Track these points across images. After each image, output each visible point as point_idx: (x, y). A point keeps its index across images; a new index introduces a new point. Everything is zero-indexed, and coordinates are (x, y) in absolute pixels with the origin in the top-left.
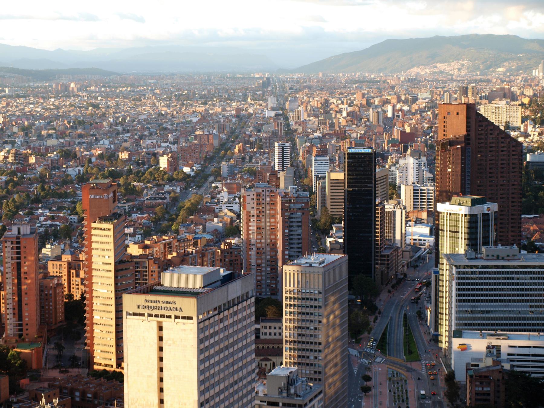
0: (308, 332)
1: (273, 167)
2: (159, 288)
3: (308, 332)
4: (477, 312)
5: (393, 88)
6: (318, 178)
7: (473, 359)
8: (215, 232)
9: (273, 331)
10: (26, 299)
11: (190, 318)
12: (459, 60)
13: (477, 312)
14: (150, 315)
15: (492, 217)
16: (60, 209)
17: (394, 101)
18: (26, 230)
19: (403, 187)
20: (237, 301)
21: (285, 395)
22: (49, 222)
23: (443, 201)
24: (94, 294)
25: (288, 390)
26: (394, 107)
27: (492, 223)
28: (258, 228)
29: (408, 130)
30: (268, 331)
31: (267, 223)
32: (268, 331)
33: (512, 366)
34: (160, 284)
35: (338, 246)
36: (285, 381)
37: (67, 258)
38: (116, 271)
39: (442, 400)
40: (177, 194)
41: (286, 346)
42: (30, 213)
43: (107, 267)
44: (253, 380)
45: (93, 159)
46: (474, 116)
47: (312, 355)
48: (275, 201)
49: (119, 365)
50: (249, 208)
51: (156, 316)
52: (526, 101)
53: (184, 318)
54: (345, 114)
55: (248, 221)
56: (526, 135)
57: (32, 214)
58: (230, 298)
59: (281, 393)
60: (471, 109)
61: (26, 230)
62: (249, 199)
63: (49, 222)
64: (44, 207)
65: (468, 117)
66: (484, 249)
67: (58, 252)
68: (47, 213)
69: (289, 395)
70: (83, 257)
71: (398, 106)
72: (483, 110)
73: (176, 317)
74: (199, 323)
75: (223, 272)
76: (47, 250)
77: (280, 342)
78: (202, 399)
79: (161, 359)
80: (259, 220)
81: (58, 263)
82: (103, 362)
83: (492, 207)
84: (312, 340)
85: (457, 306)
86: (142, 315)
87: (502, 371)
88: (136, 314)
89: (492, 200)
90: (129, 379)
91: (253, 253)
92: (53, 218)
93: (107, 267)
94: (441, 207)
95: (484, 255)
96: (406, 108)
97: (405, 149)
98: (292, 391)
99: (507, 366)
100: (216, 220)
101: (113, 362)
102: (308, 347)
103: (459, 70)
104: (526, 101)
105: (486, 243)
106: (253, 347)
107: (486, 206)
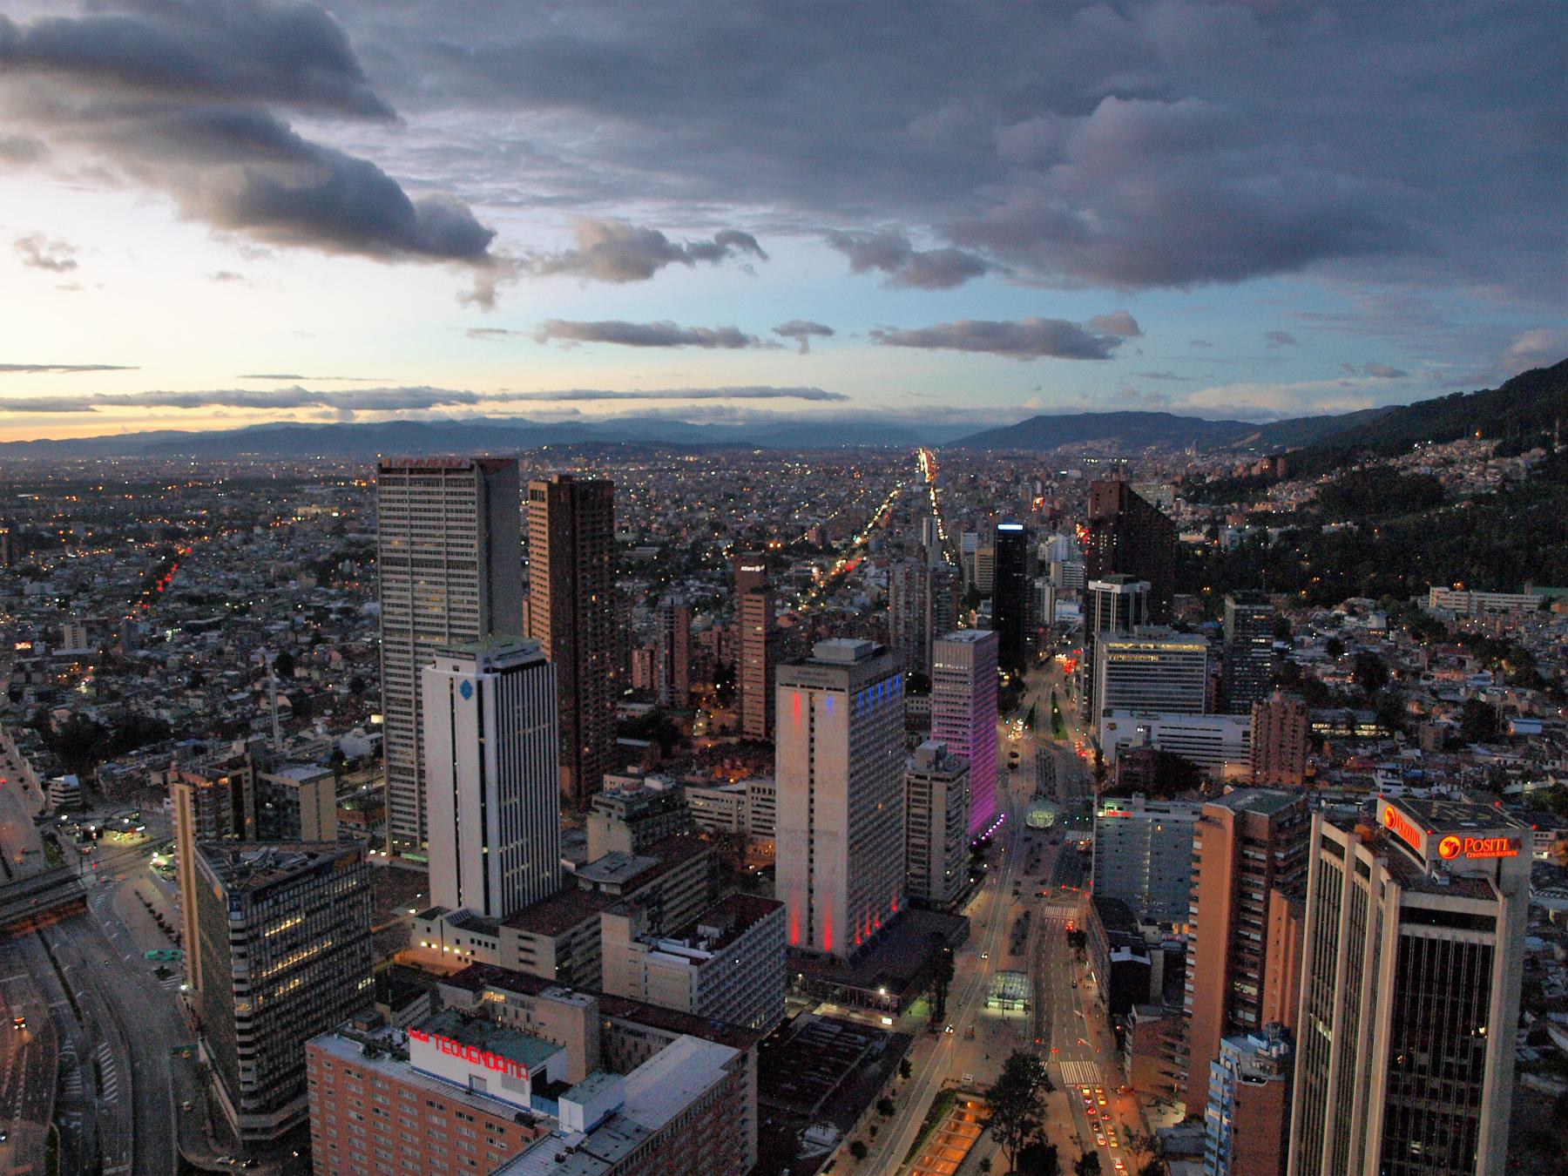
0: (957, 708)
1: (921, 543)
2: (811, 660)
3: (957, 708)
4: (1127, 692)
5: (1042, 464)
6: (966, 554)
7: (1122, 739)
8: (863, 607)
9: (919, 705)
10: (759, 629)
11: (843, 690)
12: (1109, 436)
13: (1127, 692)
14: (802, 686)
15: (1144, 597)
16: (711, 580)
17: (1044, 478)
18: (679, 600)
19: (1052, 565)
20: (885, 676)
21: (933, 768)
22: (700, 593)
23: (1095, 579)
24: (745, 664)
25: (936, 764)
26: (1043, 484)
27: (1144, 602)
28: (907, 603)
29: (1057, 507)
30: (915, 705)
31: (916, 598)
32: (915, 705)
33: (1163, 747)
34: (812, 656)
35: (986, 623)
36: (934, 754)
37: (717, 628)
38: (766, 643)
39: (1169, 803)
40: (96, 1102)
41: (935, 722)
42: (681, 584)
43: (758, 639)
44: (903, 753)
45: (743, 532)
46: (1125, 492)
47: (960, 730)
48: (199, 839)
49: (767, 734)
50: (898, 582)
51: (809, 687)
52: (1178, 479)
53: (835, 690)
54: (993, 490)
55: (897, 596)
56: (1178, 514)
57: (683, 584)
58: (881, 671)
59: (929, 767)
60: (1123, 486)
61: (679, 600)
62: (898, 574)
63: (700, 593)
64: (697, 578)
65: (1121, 496)
66: (1136, 628)
67: (708, 623)
68: (698, 583)
69: (937, 769)
70: (734, 627)
71: (1048, 483)
72: (1136, 487)
73: (829, 689)
74: (850, 695)
75: (875, 646)
76: (698, 621)
77: (929, 716)
78: (852, 770)
79: (812, 730)
80: (907, 596)
81: (708, 633)
82: (751, 730)
83: (1141, 587)
84: (961, 715)
85: (1107, 685)
86: (795, 686)
87: (1153, 752)
88: (788, 685)
89: (1144, 579)
90: (515, 388)
91: (901, 627)
92: (702, 589)
93: (758, 639)
94: (1092, 585)
95: (1135, 635)
96: (1055, 485)
97: (1055, 526)
98: (941, 765)
99: (1157, 747)
100: (863, 594)
101: (762, 731)
102: (957, 722)
103: (1110, 447)
104: (1178, 479)
105: (1137, 622)
106: (903, 720)
107: (1138, 585)
